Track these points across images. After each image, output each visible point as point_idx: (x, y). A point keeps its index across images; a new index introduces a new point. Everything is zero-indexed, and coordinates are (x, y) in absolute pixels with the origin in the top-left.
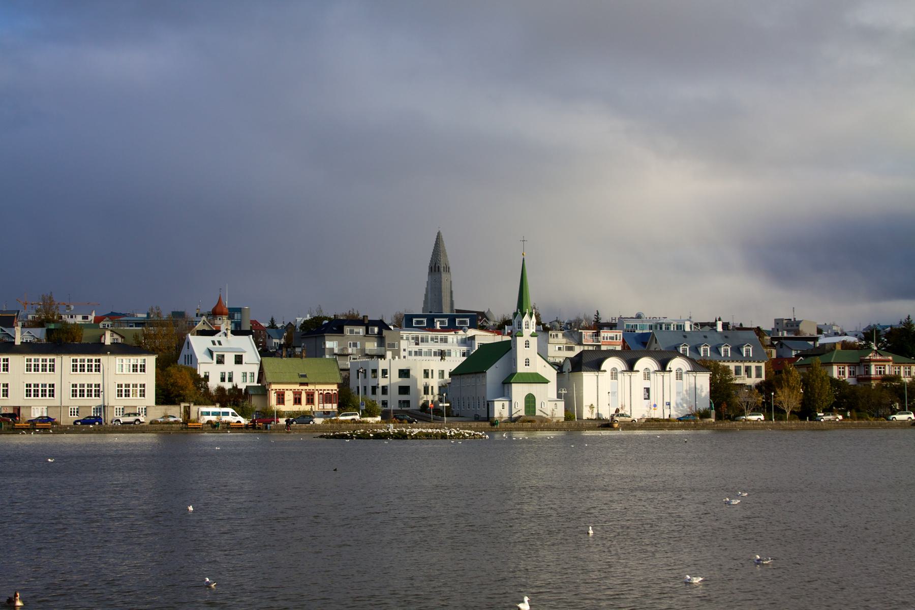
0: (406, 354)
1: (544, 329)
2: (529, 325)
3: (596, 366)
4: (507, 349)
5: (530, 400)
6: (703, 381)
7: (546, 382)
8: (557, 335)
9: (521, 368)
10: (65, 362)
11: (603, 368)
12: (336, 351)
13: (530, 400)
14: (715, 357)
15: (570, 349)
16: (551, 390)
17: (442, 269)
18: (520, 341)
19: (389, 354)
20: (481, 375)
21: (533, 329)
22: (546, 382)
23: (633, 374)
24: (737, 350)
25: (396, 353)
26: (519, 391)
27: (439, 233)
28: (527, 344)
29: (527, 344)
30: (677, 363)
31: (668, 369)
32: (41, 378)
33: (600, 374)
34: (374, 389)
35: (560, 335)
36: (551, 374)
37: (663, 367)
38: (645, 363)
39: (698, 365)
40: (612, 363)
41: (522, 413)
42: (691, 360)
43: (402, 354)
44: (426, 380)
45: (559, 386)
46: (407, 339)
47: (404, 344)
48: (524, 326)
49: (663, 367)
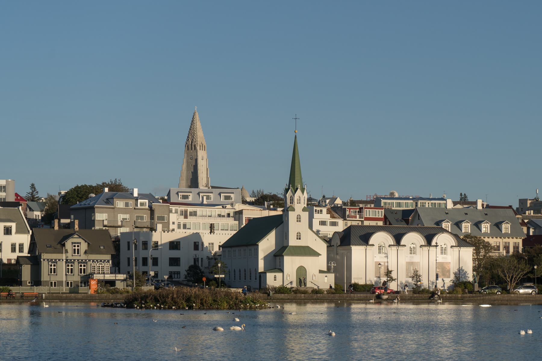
0: (175, 227)
1: (312, 205)
2: (300, 199)
3: (365, 239)
4: (279, 223)
5: (301, 272)
6: (467, 256)
7: (318, 255)
8: (321, 211)
9: (293, 242)
10: (202, 270)
11: (371, 242)
12: (106, 223)
13: (301, 272)
14: (476, 233)
15: (334, 224)
16: (322, 262)
17: (198, 148)
18: (292, 216)
19: (159, 227)
20: (252, 248)
21: (304, 204)
22: (318, 255)
23: (400, 248)
24: (498, 225)
25: (166, 229)
26: (291, 264)
27: (33, 185)
28: (299, 219)
29: (299, 219)
30: (443, 239)
31: (433, 243)
32: (302, 201)
33: (369, 248)
34: (145, 261)
35: (325, 210)
36: (321, 248)
37: (429, 239)
38: (413, 239)
39: (463, 241)
40: (381, 238)
41: (294, 285)
42: (456, 236)
43: (172, 227)
44: (196, 252)
45: (329, 259)
46: (176, 212)
47: (173, 217)
48: (296, 201)
49: (429, 239)
